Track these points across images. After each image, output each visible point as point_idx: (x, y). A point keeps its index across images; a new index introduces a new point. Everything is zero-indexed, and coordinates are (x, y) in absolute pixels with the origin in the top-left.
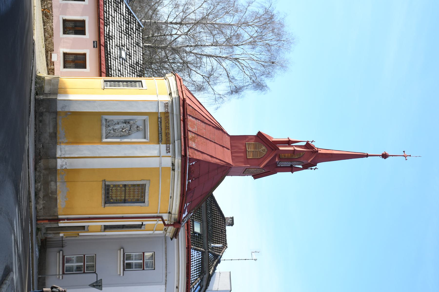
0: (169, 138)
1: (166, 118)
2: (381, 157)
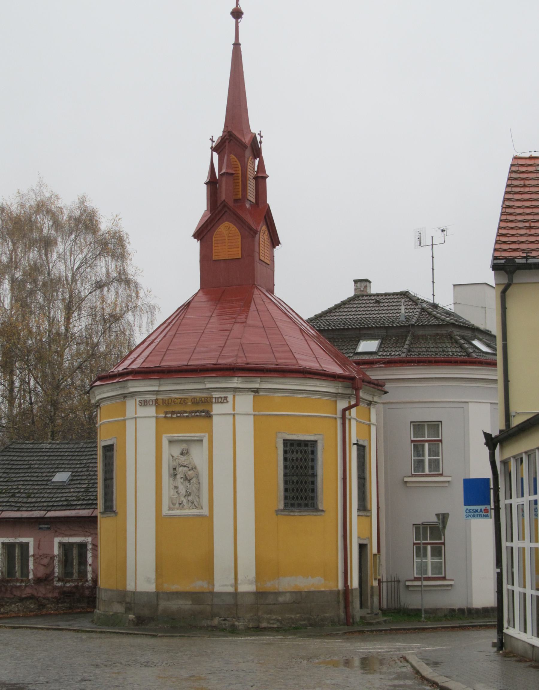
0: (201, 398)
1: (165, 403)
2: (239, 20)
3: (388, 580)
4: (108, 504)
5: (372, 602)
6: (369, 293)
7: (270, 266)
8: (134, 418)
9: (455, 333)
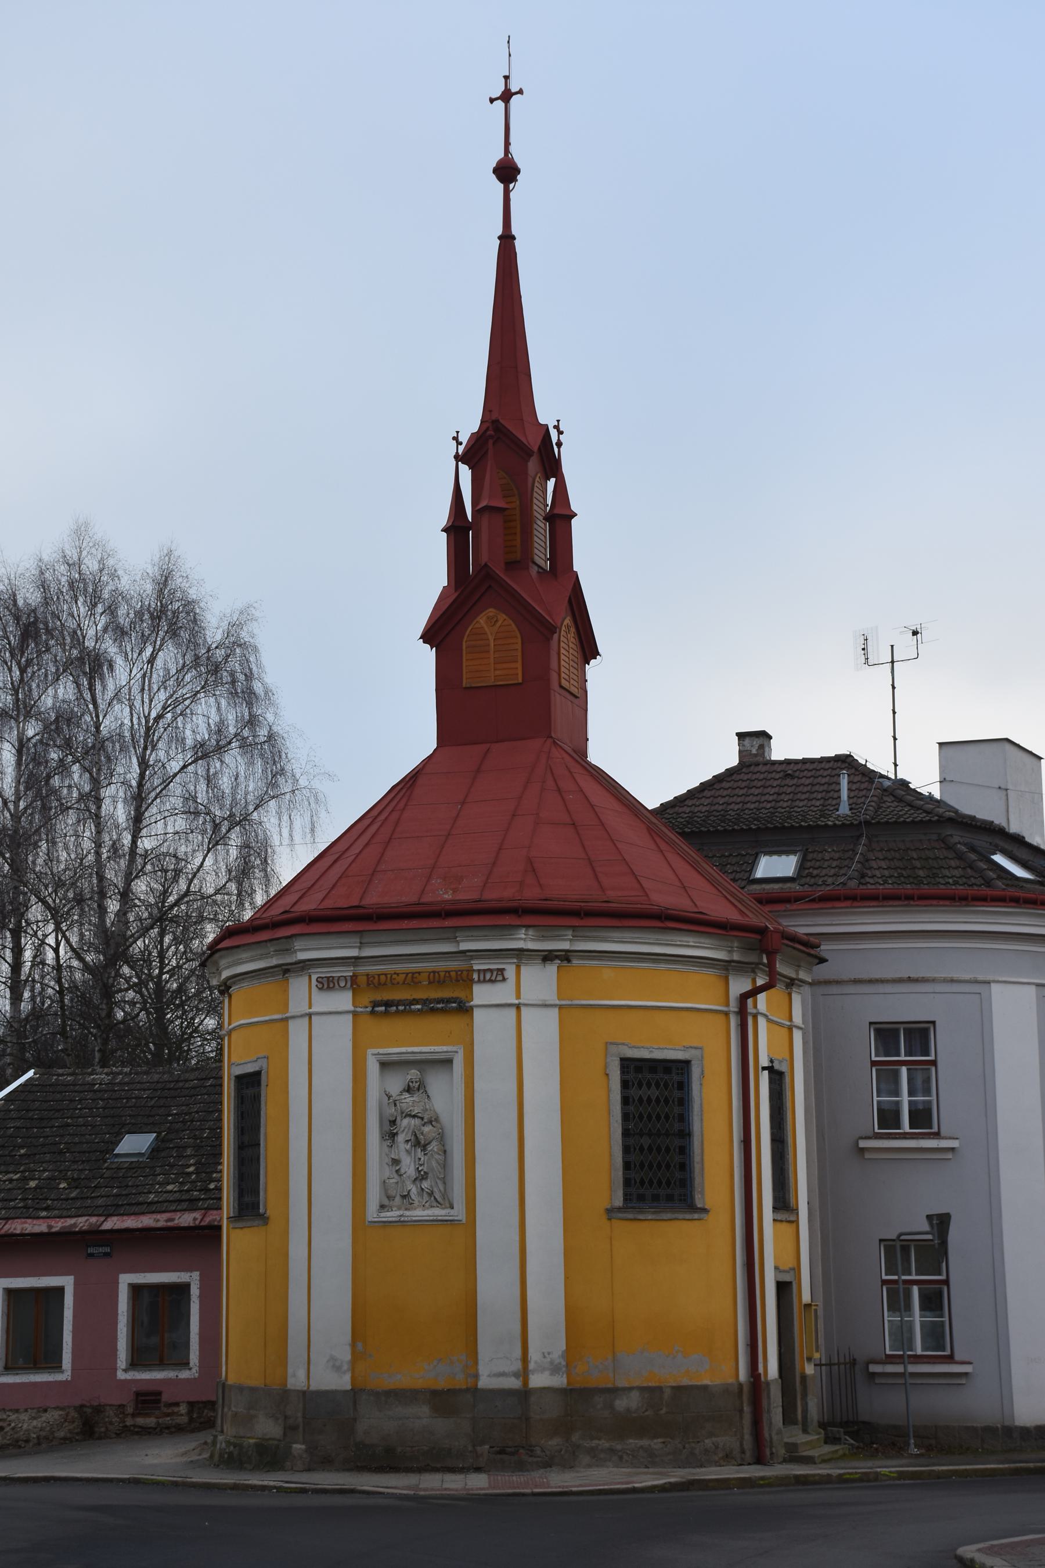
0: (449, 972)
3: (832, 1362)
4: (247, 1199)
5: (805, 1411)
6: (768, 758)
7: (579, 698)
8: (306, 1014)
9: (956, 839)
